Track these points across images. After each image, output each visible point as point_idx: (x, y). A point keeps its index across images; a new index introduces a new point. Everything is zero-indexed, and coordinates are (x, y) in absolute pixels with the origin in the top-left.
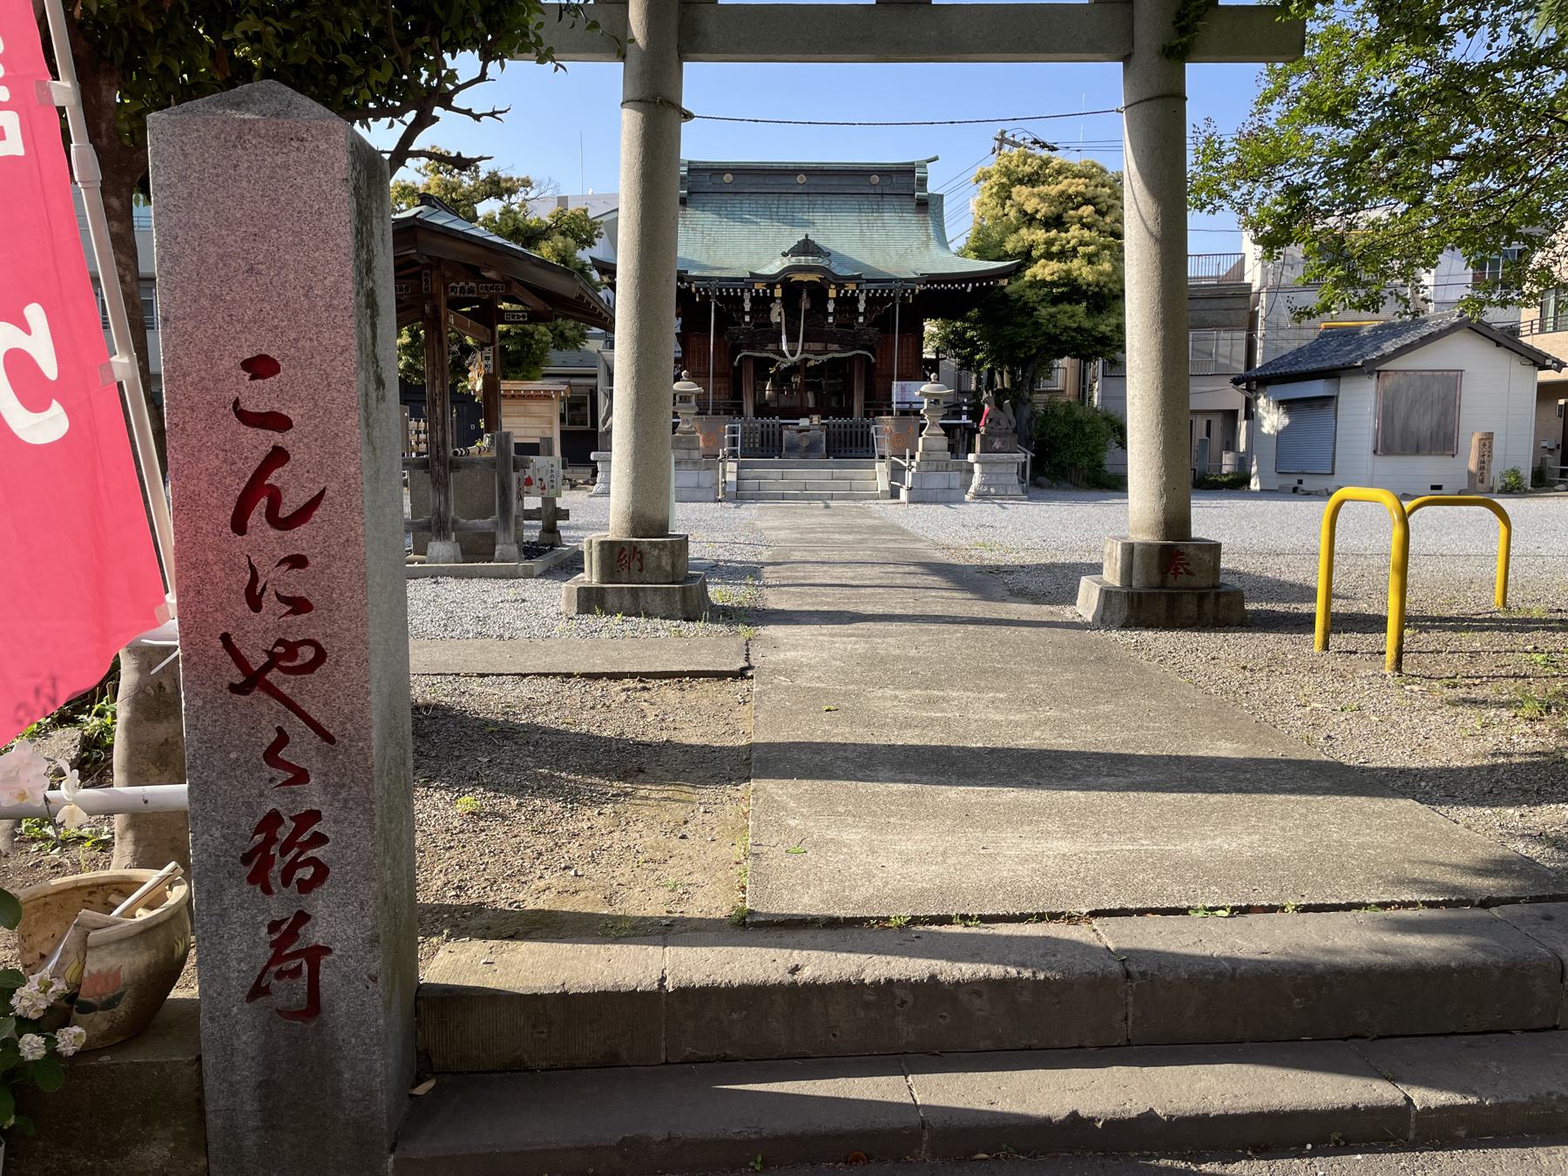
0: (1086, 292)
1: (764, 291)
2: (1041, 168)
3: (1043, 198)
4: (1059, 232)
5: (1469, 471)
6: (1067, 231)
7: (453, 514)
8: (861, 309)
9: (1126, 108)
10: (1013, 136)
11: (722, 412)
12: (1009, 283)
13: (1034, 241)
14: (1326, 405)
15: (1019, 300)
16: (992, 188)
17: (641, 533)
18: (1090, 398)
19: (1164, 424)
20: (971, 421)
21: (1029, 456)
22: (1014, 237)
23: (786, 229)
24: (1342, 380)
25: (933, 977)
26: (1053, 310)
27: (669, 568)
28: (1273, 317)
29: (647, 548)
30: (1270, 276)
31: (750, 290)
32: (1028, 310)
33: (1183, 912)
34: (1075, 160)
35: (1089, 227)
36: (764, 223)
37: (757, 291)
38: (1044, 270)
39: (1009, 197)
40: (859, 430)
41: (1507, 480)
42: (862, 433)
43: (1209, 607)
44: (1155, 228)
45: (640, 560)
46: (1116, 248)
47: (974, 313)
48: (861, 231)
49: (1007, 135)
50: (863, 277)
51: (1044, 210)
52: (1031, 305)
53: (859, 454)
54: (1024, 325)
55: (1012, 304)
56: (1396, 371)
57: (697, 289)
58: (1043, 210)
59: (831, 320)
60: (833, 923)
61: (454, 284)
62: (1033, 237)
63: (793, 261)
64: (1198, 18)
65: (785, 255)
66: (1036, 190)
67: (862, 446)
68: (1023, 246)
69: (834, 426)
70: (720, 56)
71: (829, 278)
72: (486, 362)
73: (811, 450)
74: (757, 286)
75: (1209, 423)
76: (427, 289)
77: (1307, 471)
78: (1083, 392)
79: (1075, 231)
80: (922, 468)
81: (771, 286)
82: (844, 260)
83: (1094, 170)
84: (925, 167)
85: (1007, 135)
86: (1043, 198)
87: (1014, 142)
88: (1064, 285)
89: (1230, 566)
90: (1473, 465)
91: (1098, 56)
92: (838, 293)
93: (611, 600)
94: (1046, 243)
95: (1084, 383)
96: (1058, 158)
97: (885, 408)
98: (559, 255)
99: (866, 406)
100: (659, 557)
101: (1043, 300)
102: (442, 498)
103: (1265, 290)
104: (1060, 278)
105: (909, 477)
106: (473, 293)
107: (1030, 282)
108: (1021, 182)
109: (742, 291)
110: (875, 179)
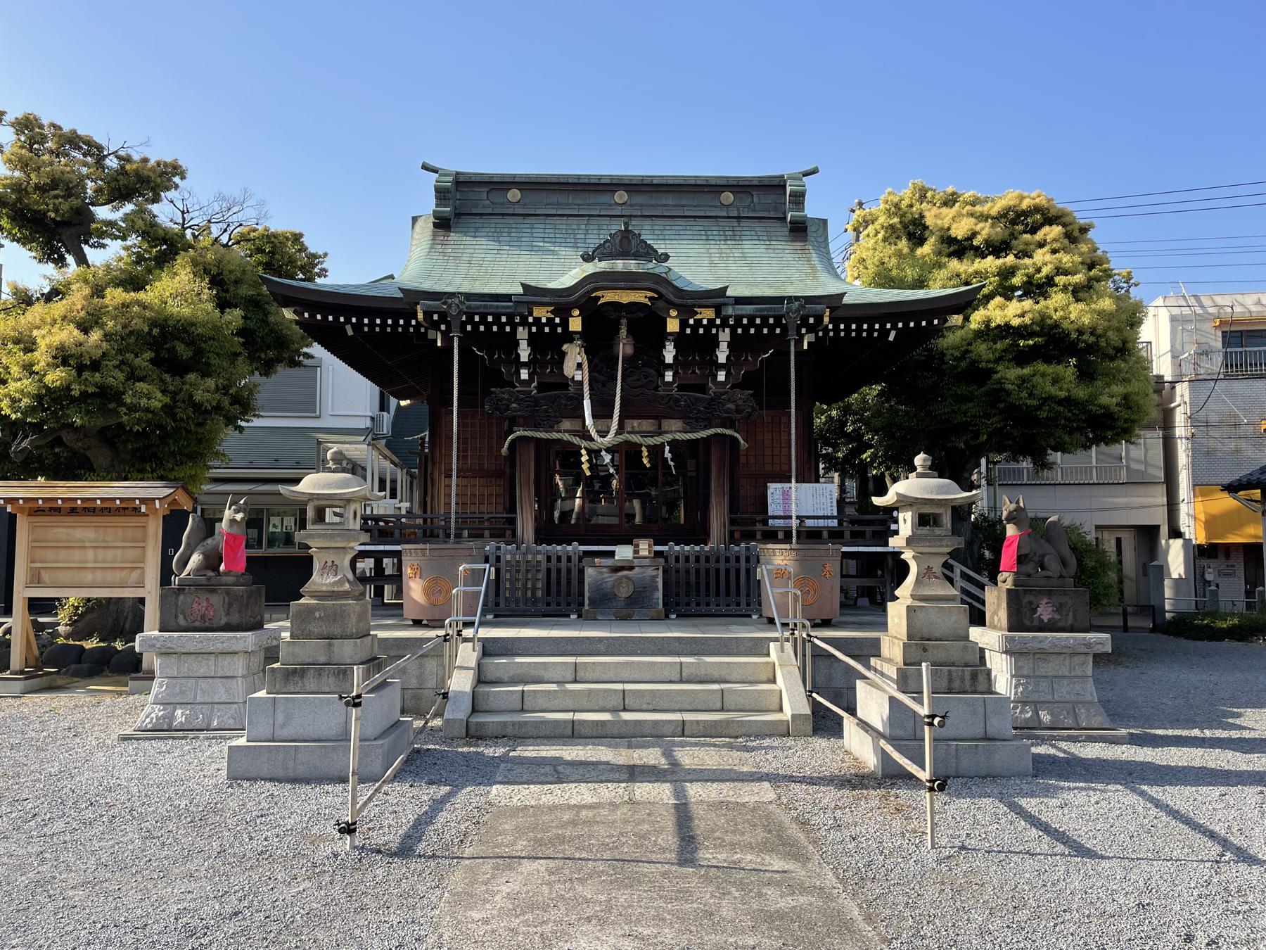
8: (722, 358)
11: (487, 533)
15: (963, 357)
16: (877, 233)
32: (979, 374)
40: (722, 566)
42: (728, 571)
48: (711, 262)
52: (983, 365)
59: (669, 376)
65: (587, 258)
67: (728, 594)
69: (677, 559)
75: (1119, 541)
81: (563, 311)
92: (683, 324)
97: (759, 527)
99: (732, 522)
110: (728, 197)
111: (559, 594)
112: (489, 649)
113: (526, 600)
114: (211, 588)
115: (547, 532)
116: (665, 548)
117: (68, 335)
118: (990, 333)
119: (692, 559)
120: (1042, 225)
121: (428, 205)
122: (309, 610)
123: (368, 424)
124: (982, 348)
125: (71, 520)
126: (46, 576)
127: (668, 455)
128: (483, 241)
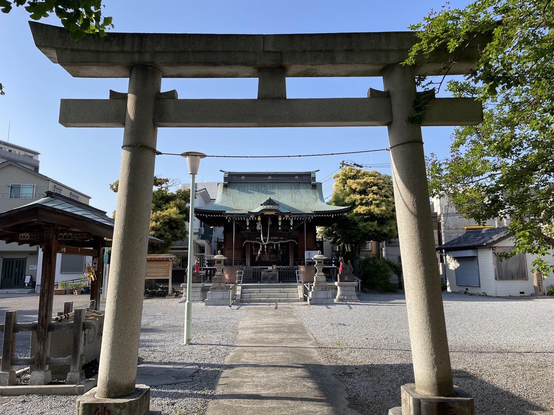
0: (377, 217)
1: (254, 218)
2: (357, 173)
3: (358, 184)
4: (365, 196)
5: (534, 286)
6: (368, 195)
7: (48, 353)
8: (292, 224)
9: (391, 148)
10: (347, 163)
11: (238, 264)
12: (347, 214)
13: (356, 199)
14: (473, 259)
15: (352, 220)
16: (340, 180)
18: (381, 253)
19: (430, 322)
20: (336, 267)
21: (360, 281)
22: (348, 198)
23: (264, 195)
24: (478, 250)
26: (365, 224)
28: (447, 224)
30: (444, 210)
31: (248, 218)
32: (356, 224)
34: (370, 170)
35: (376, 194)
36: (256, 193)
37: (251, 218)
38: (361, 209)
39: (346, 183)
40: (292, 271)
41: (549, 290)
44: (413, 210)
46: (387, 201)
47: (335, 224)
49: (345, 162)
50: (291, 213)
51: (359, 188)
52: (356, 222)
53: (292, 281)
54: (354, 229)
55: (349, 221)
56: (500, 247)
57: (228, 218)
58: (358, 188)
59: (280, 228)
61: (61, 234)
62: (355, 197)
63: (265, 207)
64: (426, 103)
65: (262, 205)
66: (355, 181)
67: (293, 277)
68: (352, 201)
69: (282, 269)
70: (176, 124)
71: (279, 213)
72: (94, 265)
73: (272, 279)
76: (46, 237)
77: (469, 285)
78: (379, 250)
79: (371, 195)
80: (316, 290)
81: (257, 217)
82: (285, 206)
83: (377, 174)
84: (315, 173)
85: (345, 162)
86: (358, 184)
87: (347, 164)
88: (368, 215)
89: (460, 367)
90: (535, 284)
91: (374, 123)
92: (282, 219)
94: (360, 200)
95: (379, 247)
96: (363, 170)
97: (302, 261)
99: (294, 260)
101: (361, 220)
102: (42, 346)
103: (442, 215)
104: (366, 212)
105: (310, 294)
106: (70, 238)
107: (355, 213)
108: (350, 178)
109: (246, 218)
110: (297, 177)
111: (256, 277)
112: (243, 288)
113: (248, 279)
115: (253, 263)
116: (279, 267)
118: (357, 214)
119: (285, 269)
120: (373, 186)
121: (222, 181)
122: (216, 278)
124: (355, 218)
125: (154, 262)
126: (148, 274)
127: (279, 246)
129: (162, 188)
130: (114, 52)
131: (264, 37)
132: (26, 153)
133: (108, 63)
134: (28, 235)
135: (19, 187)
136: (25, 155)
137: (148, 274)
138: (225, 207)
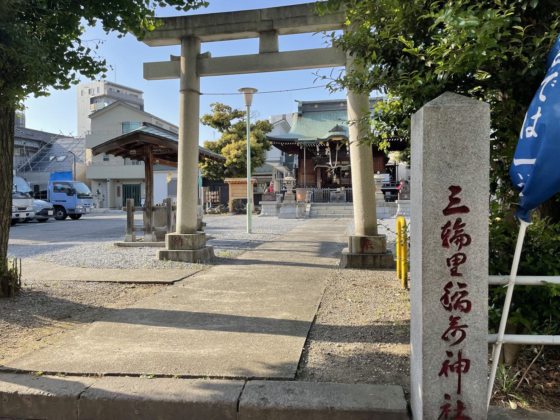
7: (153, 225)
17: (184, 232)
25: (16, 392)
27: (191, 244)
29: (183, 238)
33: (138, 376)
36: (328, 121)
43: (378, 261)
45: (182, 242)
60: (20, 372)
65: (330, 132)
74: (320, 143)
81: (325, 143)
93: (170, 255)
98: (256, 136)
100: (187, 241)
109: (315, 144)
114: (270, 195)
117: (236, 152)
121: (296, 111)
123: (280, 159)
125: (238, 185)
128: (309, 119)
129: (243, 120)
130: (170, 30)
131: (261, 10)
132: (132, 93)
133: (168, 37)
134: (135, 151)
135: (128, 124)
136: (131, 95)
137: (234, 195)
138: (298, 135)
